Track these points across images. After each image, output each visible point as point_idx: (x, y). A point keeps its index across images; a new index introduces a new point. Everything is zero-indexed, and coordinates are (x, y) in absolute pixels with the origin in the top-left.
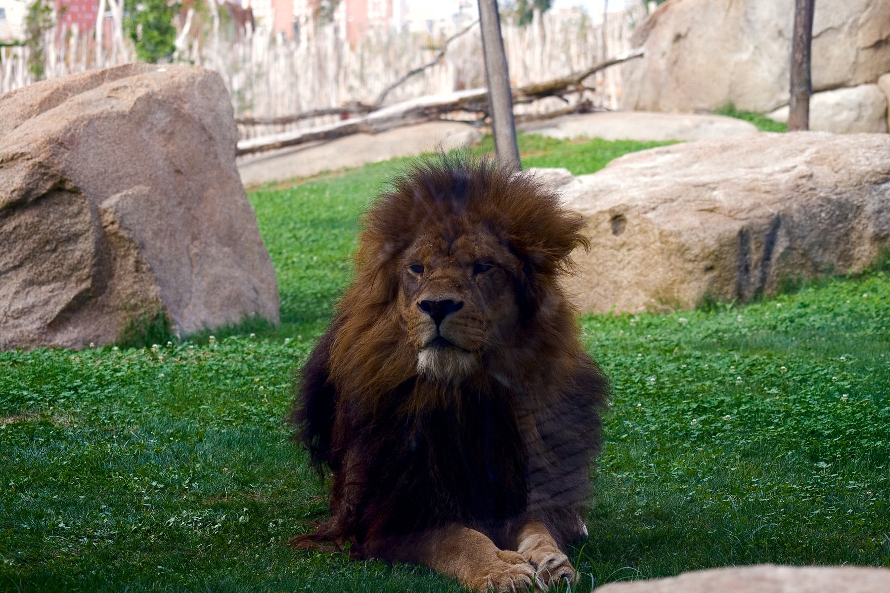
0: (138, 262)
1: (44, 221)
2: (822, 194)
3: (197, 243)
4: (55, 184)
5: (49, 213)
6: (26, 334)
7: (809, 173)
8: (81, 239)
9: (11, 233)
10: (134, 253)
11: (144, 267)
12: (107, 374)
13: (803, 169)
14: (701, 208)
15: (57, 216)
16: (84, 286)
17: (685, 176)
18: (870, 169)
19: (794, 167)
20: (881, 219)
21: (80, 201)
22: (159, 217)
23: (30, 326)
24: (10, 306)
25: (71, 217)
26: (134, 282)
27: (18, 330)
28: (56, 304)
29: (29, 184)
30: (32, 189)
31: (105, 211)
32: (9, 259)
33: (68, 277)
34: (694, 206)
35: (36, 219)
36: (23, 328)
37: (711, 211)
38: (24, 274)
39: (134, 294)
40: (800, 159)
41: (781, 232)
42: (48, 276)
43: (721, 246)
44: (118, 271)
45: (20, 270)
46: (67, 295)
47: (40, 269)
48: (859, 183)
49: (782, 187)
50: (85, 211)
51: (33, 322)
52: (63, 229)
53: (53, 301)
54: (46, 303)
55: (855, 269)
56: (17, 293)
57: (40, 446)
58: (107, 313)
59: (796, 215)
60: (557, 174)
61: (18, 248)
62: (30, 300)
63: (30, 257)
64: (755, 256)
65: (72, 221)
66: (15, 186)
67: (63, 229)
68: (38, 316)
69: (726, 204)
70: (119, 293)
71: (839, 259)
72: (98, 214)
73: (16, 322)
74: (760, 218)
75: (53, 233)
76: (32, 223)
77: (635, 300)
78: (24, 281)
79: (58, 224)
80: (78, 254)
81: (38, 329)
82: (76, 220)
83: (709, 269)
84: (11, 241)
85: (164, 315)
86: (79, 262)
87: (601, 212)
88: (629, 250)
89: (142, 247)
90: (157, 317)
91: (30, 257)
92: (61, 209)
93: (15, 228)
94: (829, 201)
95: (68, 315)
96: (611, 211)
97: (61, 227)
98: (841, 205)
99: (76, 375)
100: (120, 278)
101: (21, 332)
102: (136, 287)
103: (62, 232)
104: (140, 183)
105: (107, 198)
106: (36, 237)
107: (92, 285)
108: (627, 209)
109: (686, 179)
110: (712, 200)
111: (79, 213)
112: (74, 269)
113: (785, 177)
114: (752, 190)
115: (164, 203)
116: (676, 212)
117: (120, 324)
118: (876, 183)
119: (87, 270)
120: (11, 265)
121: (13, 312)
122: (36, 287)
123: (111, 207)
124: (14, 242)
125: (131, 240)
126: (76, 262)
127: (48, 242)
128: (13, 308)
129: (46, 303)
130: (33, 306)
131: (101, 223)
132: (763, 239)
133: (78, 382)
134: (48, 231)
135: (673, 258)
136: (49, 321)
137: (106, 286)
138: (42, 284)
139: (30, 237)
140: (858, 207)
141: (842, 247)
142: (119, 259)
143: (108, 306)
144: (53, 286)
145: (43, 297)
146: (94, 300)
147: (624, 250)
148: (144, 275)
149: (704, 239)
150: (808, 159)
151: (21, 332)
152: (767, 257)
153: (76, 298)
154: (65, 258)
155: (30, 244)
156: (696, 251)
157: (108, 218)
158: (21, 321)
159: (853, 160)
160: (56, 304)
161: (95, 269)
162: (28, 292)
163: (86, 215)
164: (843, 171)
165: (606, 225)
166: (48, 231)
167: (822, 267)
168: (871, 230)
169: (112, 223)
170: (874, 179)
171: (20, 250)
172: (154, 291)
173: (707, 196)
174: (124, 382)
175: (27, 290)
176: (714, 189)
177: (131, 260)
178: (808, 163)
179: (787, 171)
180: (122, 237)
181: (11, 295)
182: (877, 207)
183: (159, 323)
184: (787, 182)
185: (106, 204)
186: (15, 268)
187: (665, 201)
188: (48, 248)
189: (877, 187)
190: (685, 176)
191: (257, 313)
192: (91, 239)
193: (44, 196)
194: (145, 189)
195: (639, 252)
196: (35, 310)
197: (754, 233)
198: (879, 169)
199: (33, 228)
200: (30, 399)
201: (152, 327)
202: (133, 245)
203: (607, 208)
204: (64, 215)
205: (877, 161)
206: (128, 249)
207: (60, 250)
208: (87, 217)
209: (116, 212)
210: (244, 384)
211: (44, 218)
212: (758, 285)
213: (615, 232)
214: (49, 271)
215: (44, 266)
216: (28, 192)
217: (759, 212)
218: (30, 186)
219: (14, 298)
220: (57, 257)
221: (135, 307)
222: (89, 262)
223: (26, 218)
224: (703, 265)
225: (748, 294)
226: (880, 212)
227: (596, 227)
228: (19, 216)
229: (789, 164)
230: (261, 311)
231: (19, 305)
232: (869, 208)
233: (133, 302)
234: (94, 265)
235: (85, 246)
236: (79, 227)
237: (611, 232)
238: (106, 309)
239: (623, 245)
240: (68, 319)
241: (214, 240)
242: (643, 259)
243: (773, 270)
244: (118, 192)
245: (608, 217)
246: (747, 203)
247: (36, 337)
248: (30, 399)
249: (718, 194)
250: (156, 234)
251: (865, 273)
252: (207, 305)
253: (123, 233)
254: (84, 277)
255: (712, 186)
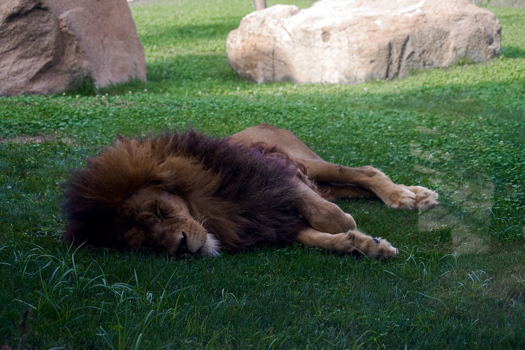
0: (78, 48)
1: (30, 25)
2: (430, 25)
3: (107, 38)
4: (36, 5)
5: (32, 20)
6: (18, 84)
7: (423, 14)
8: (49, 35)
9: (12, 30)
10: (76, 42)
11: (81, 51)
12: (82, 114)
13: (419, 11)
14: (410, 39)
15: (36, 22)
16: (49, 59)
17: (358, 12)
18: (453, 13)
19: (415, 10)
20: (458, 39)
21: (48, 14)
22: (88, 24)
23: (21, 80)
24: (10, 69)
25: (43, 23)
26: (75, 59)
27: (15, 82)
28: (35, 69)
29: (22, 5)
30: (24, 7)
31: (61, 20)
32: (10, 44)
33: (40, 55)
34: (365, 28)
35: (26, 23)
36: (17, 81)
37: (374, 31)
38: (18, 53)
39: (75, 65)
40: (417, 6)
41: (409, 44)
42: (30, 54)
43: (379, 50)
44: (67, 52)
45: (16, 50)
46: (41, 63)
47: (27, 50)
48: (448, 20)
49: (410, 20)
50: (51, 20)
51: (22, 78)
52: (39, 29)
53: (33, 67)
54: (29, 68)
55: (445, 64)
56: (14, 62)
57: (61, 158)
58: (61, 74)
59: (417, 35)
60: (292, 8)
61: (15, 38)
62: (21, 67)
63: (21, 44)
64: (395, 56)
65: (44, 25)
66: (15, 5)
67: (39, 29)
68: (25, 74)
69: (382, 28)
70: (67, 64)
71: (436, 59)
72: (58, 21)
73: (14, 78)
74: (400, 36)
75: (34, 31)
76: (23, 25)
77: (333, 76)
78: (18, 56)
79: (36, 26)
80: (46, 42)
81: (25, 82)
82: (46, 24)
83: (372, 62)
84: (12, 34)
85: (90, 77)
86: (47, 47)
87: (317, 29)
88: (331, 50)
89: (79, 40)
90: (86, 77)
91: (21, 44)
92: (39, 18)
93: (14, 28)
94: (433, 28)
95: (40, 75)
96: (322, 29)
97: (38, 28)
98: (439, 31)
99: (66, 113)
100: (68, 56)
101: (16, 83)
102: (76, 61)
103: (39, 31)
104: (79, 6)
105: (62, 13)
106: (25, 33)
107: (53, 59)
108: (331, 28)
109: (359, 14)
110: (376, 25)
111: (48, 21)
112: (44, 50)
113: (411, 15)
114: (394, 21)
115: (91, 17)
116: (356, 31)
117: (66, 80)
118: (456, 20)
119: (51, 51)
120: (11, 48)
121: (12, 72)
122: (24, 60)
123: (65, 18)
124: (14, 35)
125: (74, 36)
126: (45, 46)
127: (31, 36)
128: (12, 70)
129: (29, 68)
130: (22, 70)
131: (59, 26)
132: (400, 46)
133: (67, 117)
134: (31, 30)
135: (354, 56)
136: (30, 78)
137: (60, 60)
138: (27, 58)
139: (22, 33)
140: (447, 33)
141: (438, 53)
142: (67, 46)
143: (61, 71)
144: (33, 59)
145: (27, 65)
146: (53, 68)
147: (328, 50)
148: (80, 55)
149: (371, 46)
150: (421, 6)
151: (16, 83)
152: (401, 57)
153: (45, 66)
154: (39, 44)
155: (22, 36)
156: (367, 52)
157: (63, 24)
158: (16, 77)
159: (445, 8)
160: (35, 69)
161: (55, 51)
162: (20, 63)
163: (51, 22)
164: (440, 14)
165: (319, 36)
166: (31, 30)
167: (509, 83)
168: (452, 46)
169: (65, 27)
170: (455, 19)
171: (17, 40)
172: (85, 64)
173: (372, 23)
174: (92, 117)
175: (19, 61)
176: (375, 20)
177: (74, 47)
178: (421, 8)
179: (411, 12)
180: (69, 35)
181: (11, 64)
182: (456, 33)
183: (88, 80)
184: (412, 18)
185: (62, 16)
186: (14, 49)
187: (350, 25)
188: (31, 39)
189: (456, 22)
190: (358, 12)
191: (136, 76)
192: (54, 35)
193: (30, 11)
194: (82, 9)
195: (336, 51)
196: (24, 71)
197: (396, 44)
198: (458, 14)
199: (23, 28)
200: (44, 126)
201: (84, 83)
202: (75, 38)
203: (320, 27)
204: (40, 22)
205: (456, 9)
206: (73, 40)
207: (37, 40)
208: (52, 23)
209: (67, 21)
210: (159, 121)
211: (29, 23)
212: (396, 71)
213: (324, 40)
214: (31, 51)
215: (29, 48)
216: (22, 9)
217: (398, 33)
218: (23, 6)
219: (12, 65)
220: (35, 44)
221: (75, 72)
222: (52, 47)
223: (20, 23)
224: (369, 59)
225: (391, 75)
226: (457, 35)
227: (314, 37)
228: (16, 21)
229: (412, 8)
230: (138, 75)
231: (15, 69)
232: (452, 34)
233: (74, 69)
234: (55, 49)
235: (50, 39)
236: (47, 28)
237: (321, 40)
238: (60, 72)
239: (328, 47)
240: (40, 77)
241: (115, 37)
242: (338, 55)
243: (404, 63)
244: (68, 10)
245: (321, 32)
246: (393, 28)
247: (24, 86)
248: (44, 126)
249: (378, 22)
250: (87, 33)
251: (449, 66)
252: (112, 72)
253: (70, 32)
254: (49, 55)
255: (374, 18)
